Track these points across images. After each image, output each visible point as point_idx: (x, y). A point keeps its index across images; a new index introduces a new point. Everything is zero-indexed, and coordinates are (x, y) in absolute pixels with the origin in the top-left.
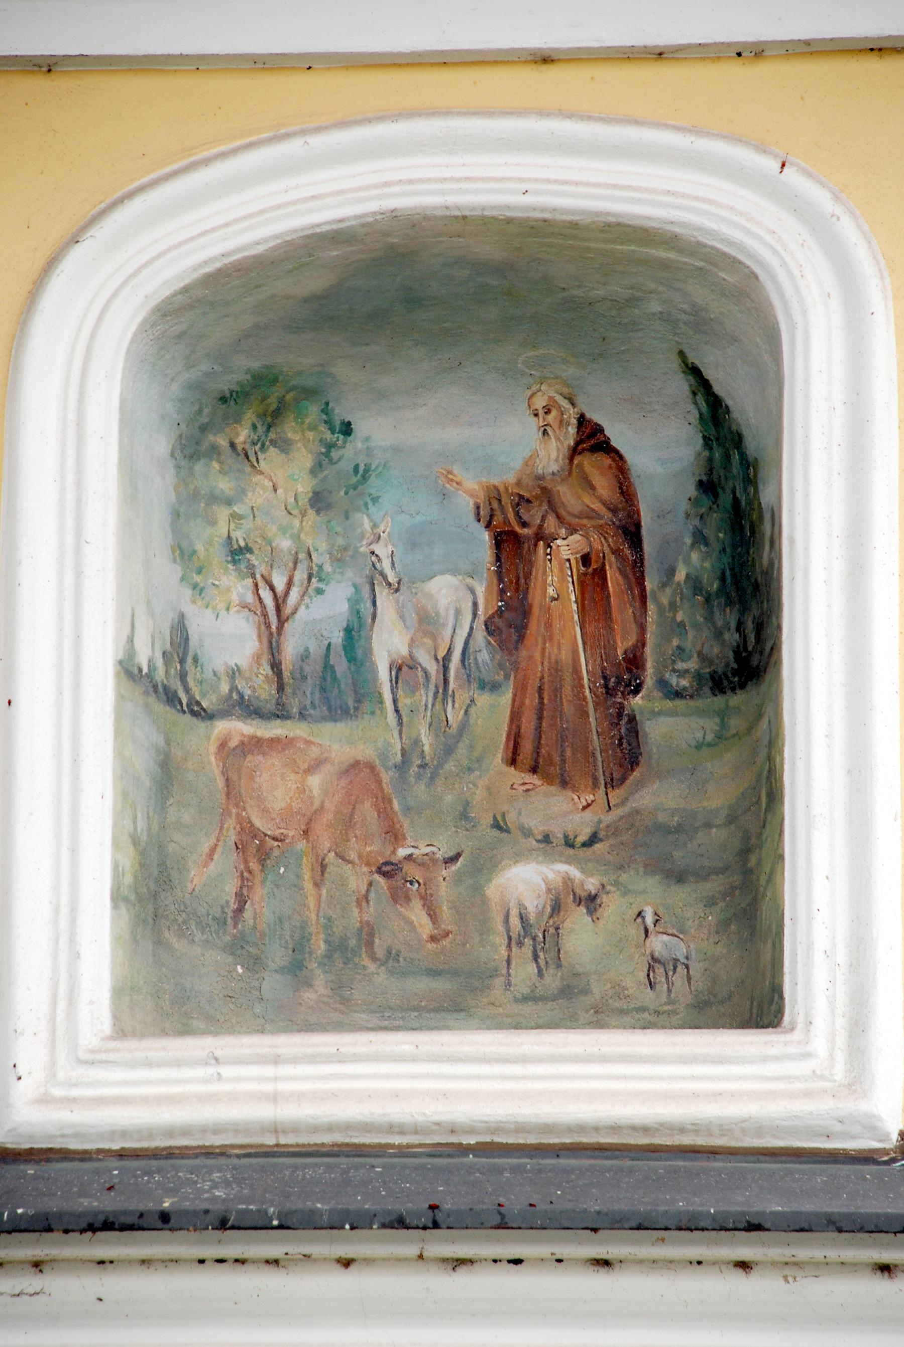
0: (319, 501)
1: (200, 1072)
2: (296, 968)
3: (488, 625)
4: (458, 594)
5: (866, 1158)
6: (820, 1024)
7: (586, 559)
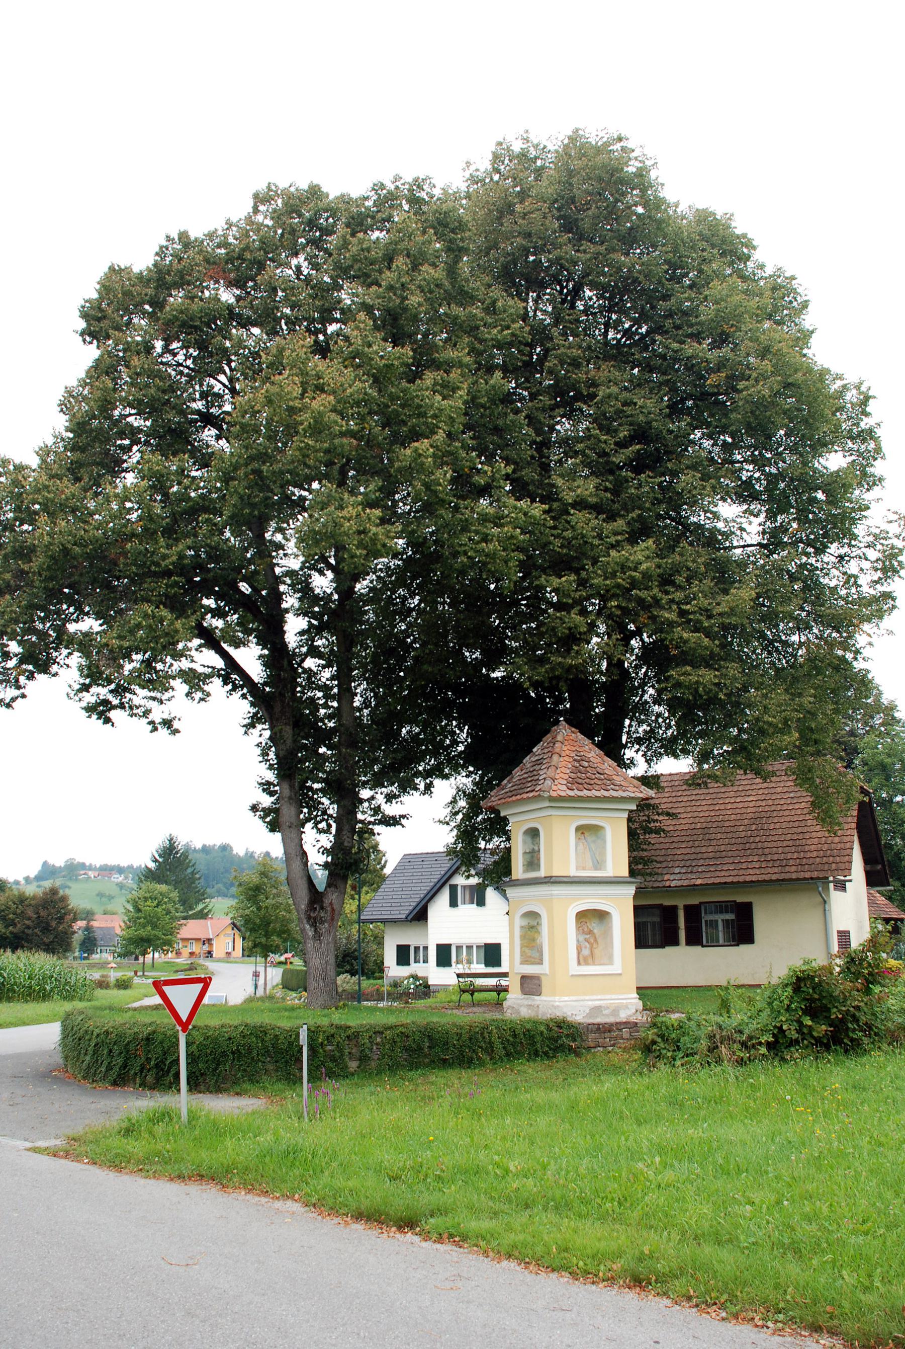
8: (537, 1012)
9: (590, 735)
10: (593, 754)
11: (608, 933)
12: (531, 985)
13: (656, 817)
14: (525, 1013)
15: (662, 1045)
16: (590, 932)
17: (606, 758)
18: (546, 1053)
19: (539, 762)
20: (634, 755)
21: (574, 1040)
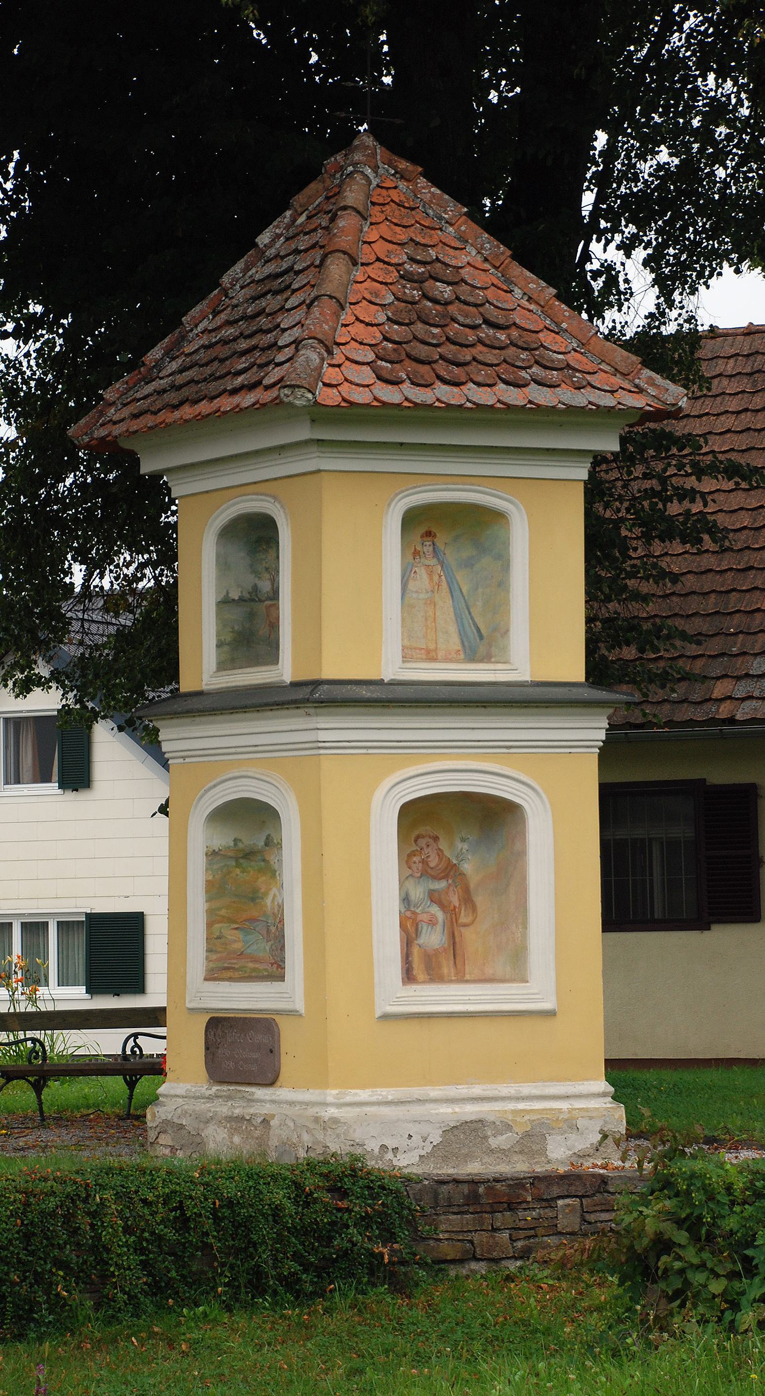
8: (262, 1141)
9: (464, 189)
10: (473, 255)
11: (510, 875)
12: (242, 1049)
13: (691, 482)
14: (219, 1142)
15: (691, 1255)
16: (450, 871)
17: (518, 271)
18: (290, 1283)
19: (278, 284)
20: (614, 255)
21: (389, 1237)
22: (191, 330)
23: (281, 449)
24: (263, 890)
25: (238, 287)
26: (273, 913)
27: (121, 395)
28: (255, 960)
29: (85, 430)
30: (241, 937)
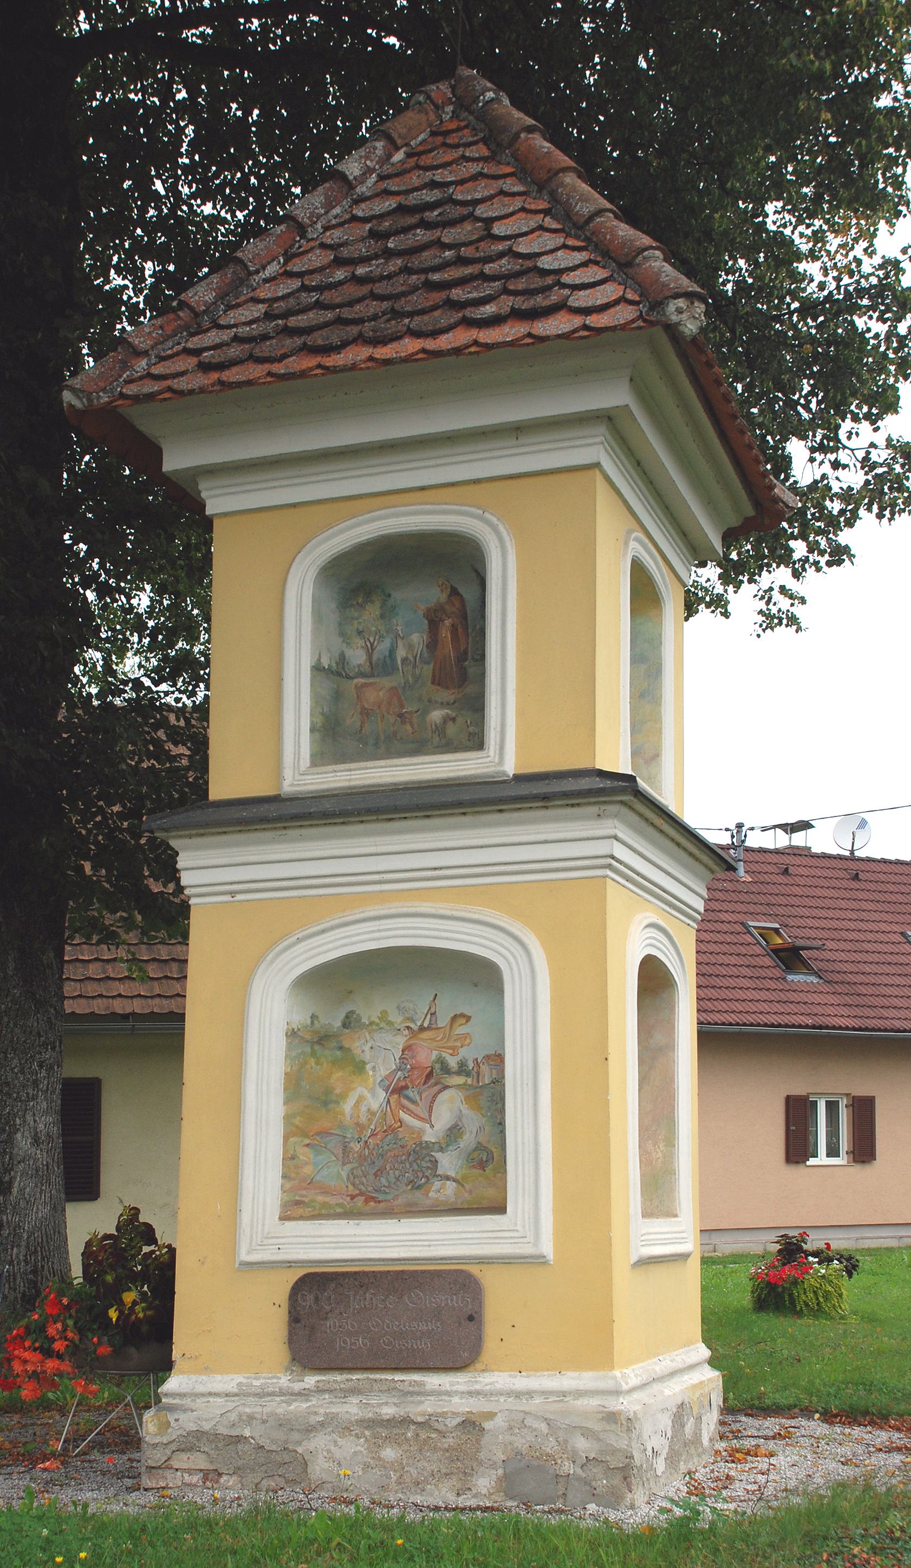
0: (382, 616)
1: (331, 775)
2: (376, 744)
3: (428, 647)
4: (418, 639)
5: (504, 782)
6: (492, 748)
7: (453, 626)
22: (257, 272)
23: (518, 430)
24: (338, 1091)
25: (319, 226)
26: (357, 1124)
27: (156, 344)
28: (326, 1191)
29: (102, 384)
30: (312, 1156)
